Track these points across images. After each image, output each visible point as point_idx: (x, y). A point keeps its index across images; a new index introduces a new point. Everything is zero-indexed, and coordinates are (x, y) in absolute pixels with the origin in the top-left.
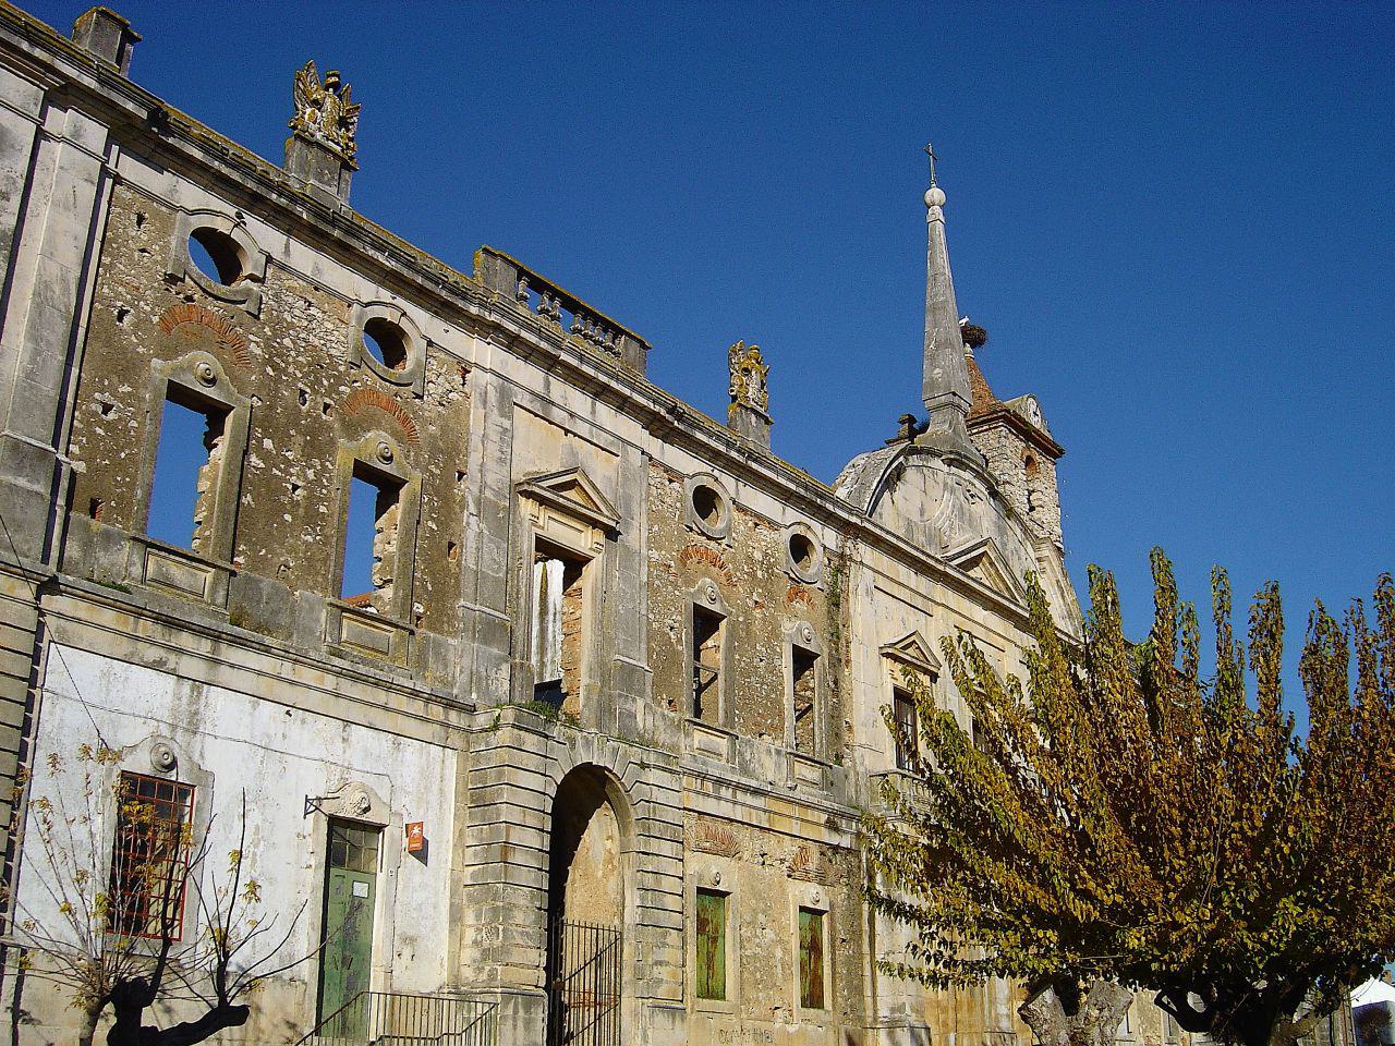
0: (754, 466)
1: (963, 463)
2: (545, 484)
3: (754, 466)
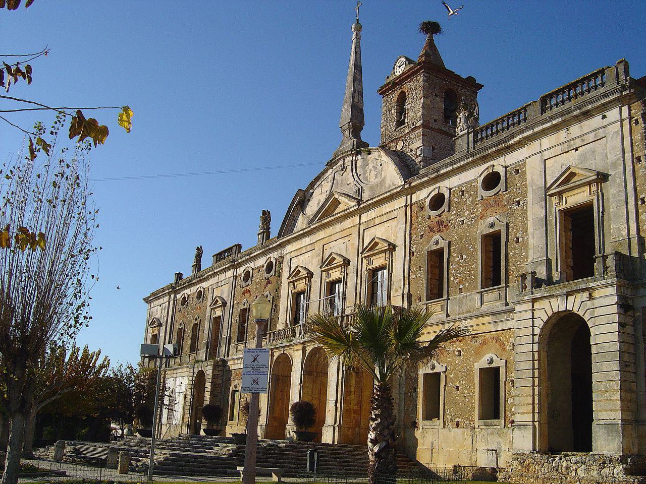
0: (251, 256)
1: (334, 162)
2: (365, 252)
3: (251, 256)
